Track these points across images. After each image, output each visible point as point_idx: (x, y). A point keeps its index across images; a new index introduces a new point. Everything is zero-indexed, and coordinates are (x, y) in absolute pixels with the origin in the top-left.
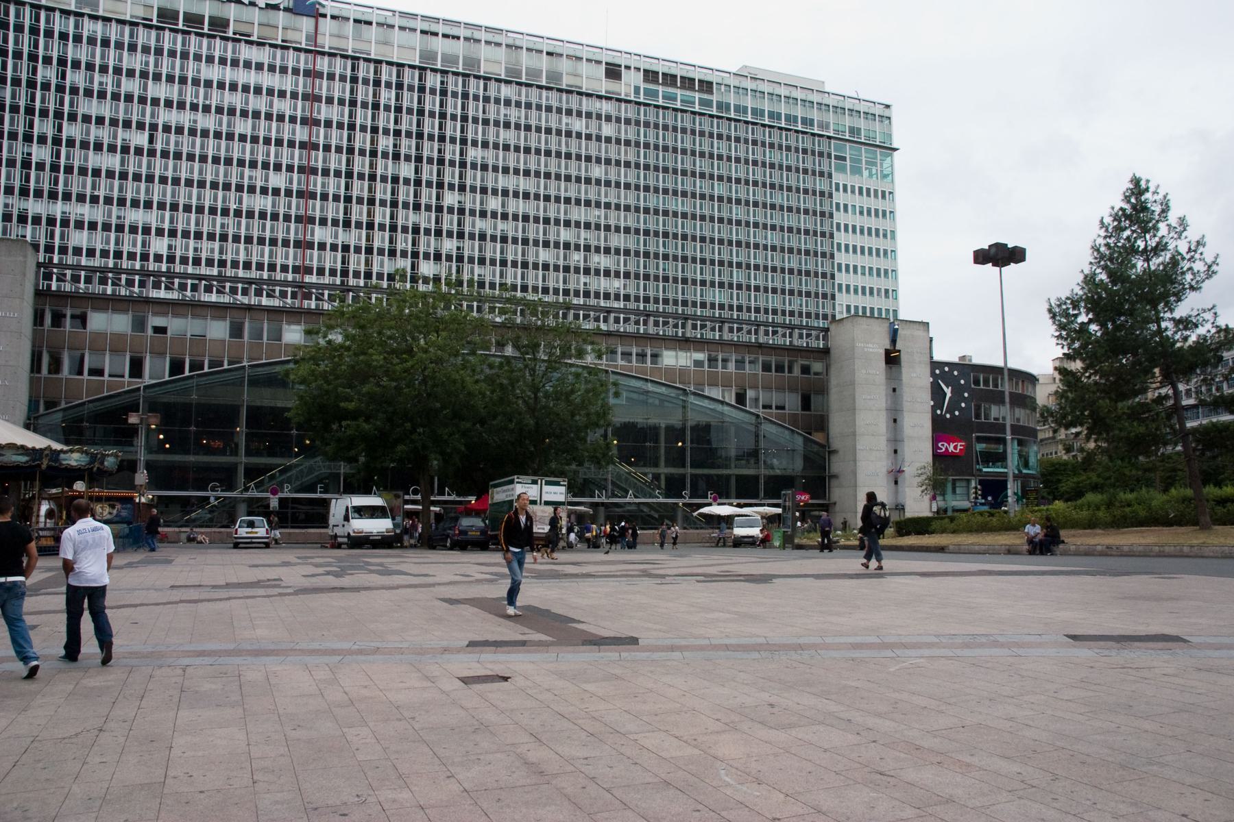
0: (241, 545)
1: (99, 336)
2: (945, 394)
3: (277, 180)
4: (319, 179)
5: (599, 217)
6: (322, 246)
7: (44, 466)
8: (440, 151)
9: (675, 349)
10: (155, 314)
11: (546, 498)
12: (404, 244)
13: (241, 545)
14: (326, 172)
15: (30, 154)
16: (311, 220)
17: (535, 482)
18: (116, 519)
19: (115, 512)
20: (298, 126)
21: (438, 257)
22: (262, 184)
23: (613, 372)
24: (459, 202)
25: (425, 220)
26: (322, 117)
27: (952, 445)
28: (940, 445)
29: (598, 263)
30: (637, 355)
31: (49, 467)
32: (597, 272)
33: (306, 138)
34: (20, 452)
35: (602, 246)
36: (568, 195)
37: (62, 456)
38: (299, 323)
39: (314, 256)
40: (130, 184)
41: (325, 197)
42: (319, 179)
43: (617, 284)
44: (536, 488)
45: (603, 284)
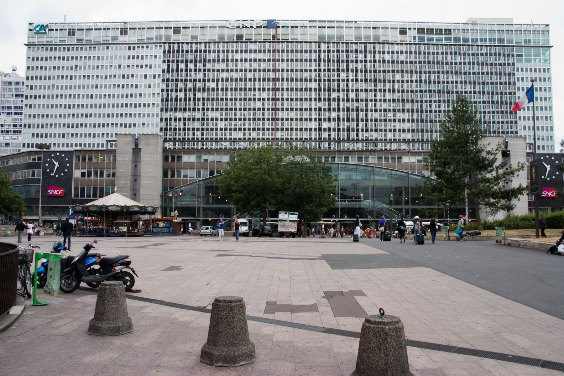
2: (55, 165)
3: (264, 95)
4: (280, 92)
5: (399, 96)
7: (125, 211)
8: (328, 76)
10: (204, 154)
11: (290, 219)
15: (177, 96)
17: (286, 214)
20: (271, 73)
26: (280, 68)
27: (56, 191)
28: (49, 191)
29: (400, 117)
30: (365, 158)
33: (274, 77)
36: (385, 88)
38: (194, 154)
42: (280, 92)
44: (286, 216)
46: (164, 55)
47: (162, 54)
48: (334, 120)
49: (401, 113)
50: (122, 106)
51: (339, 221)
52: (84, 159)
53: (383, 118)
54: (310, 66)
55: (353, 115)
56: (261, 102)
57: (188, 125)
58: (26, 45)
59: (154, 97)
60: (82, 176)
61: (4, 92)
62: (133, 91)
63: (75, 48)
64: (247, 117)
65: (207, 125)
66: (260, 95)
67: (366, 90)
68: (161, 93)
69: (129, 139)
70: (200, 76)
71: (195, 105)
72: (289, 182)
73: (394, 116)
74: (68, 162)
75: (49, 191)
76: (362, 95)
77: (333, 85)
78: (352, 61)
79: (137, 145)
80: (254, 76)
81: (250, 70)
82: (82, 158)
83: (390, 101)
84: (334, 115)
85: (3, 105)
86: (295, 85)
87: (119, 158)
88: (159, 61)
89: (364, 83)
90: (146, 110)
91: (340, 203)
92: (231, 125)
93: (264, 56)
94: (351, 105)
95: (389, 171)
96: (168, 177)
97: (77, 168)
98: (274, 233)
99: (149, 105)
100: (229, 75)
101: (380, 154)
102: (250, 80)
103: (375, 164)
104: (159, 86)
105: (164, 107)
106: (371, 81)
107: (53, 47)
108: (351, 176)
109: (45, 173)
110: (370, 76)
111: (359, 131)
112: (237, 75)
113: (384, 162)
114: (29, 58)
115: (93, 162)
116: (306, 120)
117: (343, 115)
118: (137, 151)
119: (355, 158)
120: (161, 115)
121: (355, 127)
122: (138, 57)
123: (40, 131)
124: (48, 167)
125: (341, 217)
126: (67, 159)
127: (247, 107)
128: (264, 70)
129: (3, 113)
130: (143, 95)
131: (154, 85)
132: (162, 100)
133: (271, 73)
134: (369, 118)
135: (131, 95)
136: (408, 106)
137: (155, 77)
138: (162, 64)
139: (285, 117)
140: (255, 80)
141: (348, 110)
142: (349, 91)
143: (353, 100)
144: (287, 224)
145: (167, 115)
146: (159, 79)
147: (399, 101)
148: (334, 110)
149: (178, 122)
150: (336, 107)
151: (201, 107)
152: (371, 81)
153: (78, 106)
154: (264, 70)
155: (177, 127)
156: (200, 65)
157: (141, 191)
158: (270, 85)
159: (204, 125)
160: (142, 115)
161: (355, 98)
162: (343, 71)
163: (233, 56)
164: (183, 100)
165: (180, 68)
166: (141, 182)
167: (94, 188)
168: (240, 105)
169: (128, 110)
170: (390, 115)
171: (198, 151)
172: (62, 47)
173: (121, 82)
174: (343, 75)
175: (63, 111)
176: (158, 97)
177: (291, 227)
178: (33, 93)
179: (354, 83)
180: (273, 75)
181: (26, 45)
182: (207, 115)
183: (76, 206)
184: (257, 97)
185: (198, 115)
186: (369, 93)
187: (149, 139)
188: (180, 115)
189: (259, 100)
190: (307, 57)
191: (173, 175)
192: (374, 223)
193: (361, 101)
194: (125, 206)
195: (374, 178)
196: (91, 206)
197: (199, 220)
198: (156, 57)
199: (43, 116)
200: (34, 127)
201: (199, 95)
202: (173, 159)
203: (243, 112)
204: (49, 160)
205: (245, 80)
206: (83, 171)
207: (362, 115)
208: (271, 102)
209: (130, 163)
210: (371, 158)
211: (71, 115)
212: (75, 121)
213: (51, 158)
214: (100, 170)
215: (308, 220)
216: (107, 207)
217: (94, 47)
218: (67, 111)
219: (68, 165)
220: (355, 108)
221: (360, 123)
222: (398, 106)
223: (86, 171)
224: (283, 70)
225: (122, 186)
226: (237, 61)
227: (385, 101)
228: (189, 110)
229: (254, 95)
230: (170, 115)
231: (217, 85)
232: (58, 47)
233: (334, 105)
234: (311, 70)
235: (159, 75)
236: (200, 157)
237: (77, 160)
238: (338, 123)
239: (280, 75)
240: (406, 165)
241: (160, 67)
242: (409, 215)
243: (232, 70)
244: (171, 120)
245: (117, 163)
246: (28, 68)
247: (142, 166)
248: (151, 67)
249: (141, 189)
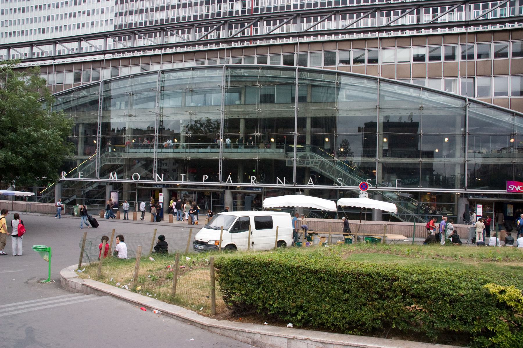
28: (510, 187)
62: (83, 19)
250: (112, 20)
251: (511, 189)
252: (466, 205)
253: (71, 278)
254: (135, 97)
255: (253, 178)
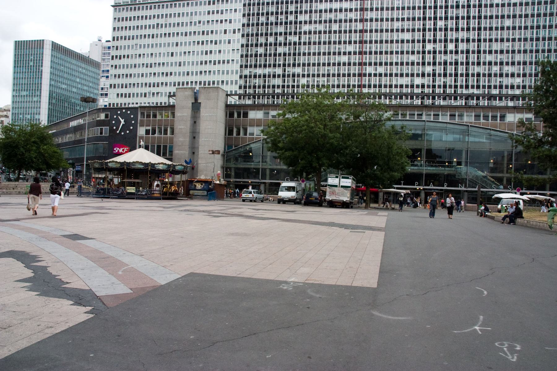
0: (246, 201)
1: (253, 120)
2: (121, 122)
3: (350, 48)
4: (368, 45)
5: (508, 47)
6: (370, 75)
7: (149, 169)
8: (424, 25)
9: (514, 113)
10: (272, 110)
11: (342, 184)
12: (407, 71)
13: (337, 206)
14: (371, 42)
15: (257, 51)
16: (365, 64)
17: (337, 177)
18: (203, 189)
19: (202, 186)
20: (358, 23)
21: (423, 75)
22: (344, 51)
23: (470, 126)
24: (434, 48)
25: (440, 58)
26: (369, 18)
27: (121, 149)
28: (115, 149)
29: (508, 71)
30: (458, 116)
31: (151, 169)
32: (507, 75)
33: (361, 28)
34: (141, 164)
35: (510, 61)
36: (491, 37)
37: (156, 165)
38: (262, 110)
39: (366, 79)
40: (322, 57)
41: (370, 53)
42: (368, 45)
43: (518, 81)
44: (337, 180)
45: (508, 81)
46: (244, 9)
47: (242, 8)
48: (429, 75)
49: (510, 66)
50: (201, 63)
51: (424, 189)
52: (148, 116)
53: (487, 72)
54: (402, 15)
55: (451, 69)
56: (347, 56)
57: (268, 82)
58: (113, 6)
59: (233, 53)
60: (146, 134)
61: (104, 56)
62: (213, 47)
63: (161, 6)
64: (331, 73)
65: (288, 82)
66: (346, 49)
67: (468, 40)
68: (240, 48)
69: (189, 93)
70: (281, 29)
71: (276, 61)
72: (349, 137)
73: (500, 70)
74: (132, 119)
75: (115, 149)
76: (462, 46)
77: (429, 36)
78: (452, 7)
79: (196, 99)
80: (340, 27)
81: (335, 21)
82: (153, 115)
83: (496, 52)
84: (429, 69)
85: (103, 69)
86: (385, 36)
87: (177, 114)
88: (239, 15)
89: (465, 32)
90: (225, 67)
91: (425, 168)
92: (314, 82)
93: (350, 6)
94: (449, 58)
95: (489, 131)
96: (233, 135)
97: (142, 125)
98: (320, 202)
99: (228, 62)
100: (312, 27)
101: (478, 111)
102: (335, 32)
103: (471, 123)
104: (238, 41)
105: (244, 64)
106: (474, 29)
107: (137, 6)
108: (441, 137)
109: (111, 130)
110: (473, 23)
111: (457, 88)
112: (321, 27)
113: (482, 120)
114: (115, 19)
115: (157, 119)
116: (396, 75)
117: (439, 69)
118: (196, 106)
119: (447, 115)
120: (241, 72)
121: (453, 84)
122: (218, 12)
123: (124, 91)
124: (114, 125)
125: (425, 185)
126: (132, 116)
127: (332, 62)
128: (351, 21)
129: (103, 76)
130: (222, 51)
131: (234, 40)
132: (242, 56)
133: (358, 23)
134: (470, 72)
135: (211, 52)
136: (518, 58)
137: (234, 32)
138: (242, 18)
139: (373, 72)
140: (340, 32)
141: (445, 63)
142: (447, 42)
143: (451, 52)
144: (337, 191)
145: (247, 72)
146: (239, 34)
147: (508, 52)
148: (429, 64)
149: (257, 79)
150: (432, 61)
151: (281, 63)
152: (474, 29)
153: (159, 64)
154: (351, 21)
155: (257, 85)
156: (282, 17)
157: (200, 149)
158: (356, 37)
159: (284, 82)
160: (221, 72)
161: (454, 50)
162: (441, 19)
163: (317, 7)
164: (263, 55)
165: (260, 22)
166: (200, 140)
167: (157, 146)
168: (323, 59)
169: (208, 68)
170: (495, 69)
171: (264, 105)
172: (145, 6)
173: (201, 38)
174: (441, 24)
175: (145, 70)
176: (238, 53)
177: (343, 195)
178: (118, 53)
179: (454, 32)
180: (360, 26)
181: (113, 6)
182: (288, 72)
183: (94, 162)
184: (342, 51)
185: (279, 71)
186: (471, 43)
187: (209, 93)
188: (259, 71)
189: (345, 53)
190: (399, 4)
191: (238, 133)
192: (466, 193)
193: (461, 53)
194: (150, 163)
195: (468, 139)
196: (110, 162)
197: (264, 183)
198: (236, 10)
199: (127, 76)
200: (119, 87)
201: (280, 50)
202: (239, 116)
203: (326, 68)
204: (115, 117)
205: (330, 32)
206: (148, 128)
207: (461, 69)
208: (357, 56)
209: (189, 119)
210: (467, 116)
211: (153, 74)
212: (156, 80)
213: (117, 115)
214: (164, 127)
215: (372, 186)
216: (129, 164)
217: (175, 4)
218: (149, 70)
219: (133, 122)
220: (453, 61)
221: (459, 78)
222: (504, 57)
223: (150, 128)
224: (371, 20)
225: (180, 144)
226: (321, 11)
227: (490, 52)
228: (270, 66)
229: (339, 49)
230: (250, 72)
231: (299, 39)
232: (141, 6)
233: (429, 58)
234: (403, 19)
235: (239, 30)
236: (268, 113)
237: (142, 117)
238: (433, 79)
239: (368, 26)
240: (510, 124)
241: (239, 21)
242: (511, 185)
243: (315, 22)
244: (250, 77)
245: (176, 119)
246: (114, 29)
247: (201, 123)
248: (230, 22)
249: (200, 147)
250: (238, 50)
251: (116, 151)
252: (520, 205)
253: (275, 278)
254: (492, 137)
255: (417, 183)
